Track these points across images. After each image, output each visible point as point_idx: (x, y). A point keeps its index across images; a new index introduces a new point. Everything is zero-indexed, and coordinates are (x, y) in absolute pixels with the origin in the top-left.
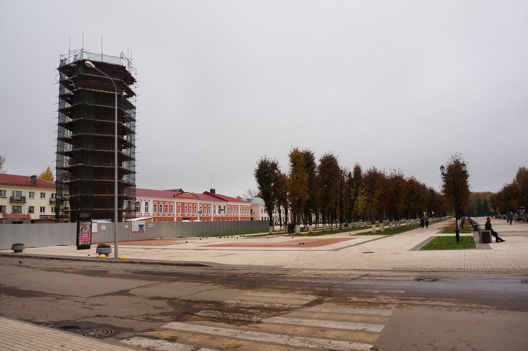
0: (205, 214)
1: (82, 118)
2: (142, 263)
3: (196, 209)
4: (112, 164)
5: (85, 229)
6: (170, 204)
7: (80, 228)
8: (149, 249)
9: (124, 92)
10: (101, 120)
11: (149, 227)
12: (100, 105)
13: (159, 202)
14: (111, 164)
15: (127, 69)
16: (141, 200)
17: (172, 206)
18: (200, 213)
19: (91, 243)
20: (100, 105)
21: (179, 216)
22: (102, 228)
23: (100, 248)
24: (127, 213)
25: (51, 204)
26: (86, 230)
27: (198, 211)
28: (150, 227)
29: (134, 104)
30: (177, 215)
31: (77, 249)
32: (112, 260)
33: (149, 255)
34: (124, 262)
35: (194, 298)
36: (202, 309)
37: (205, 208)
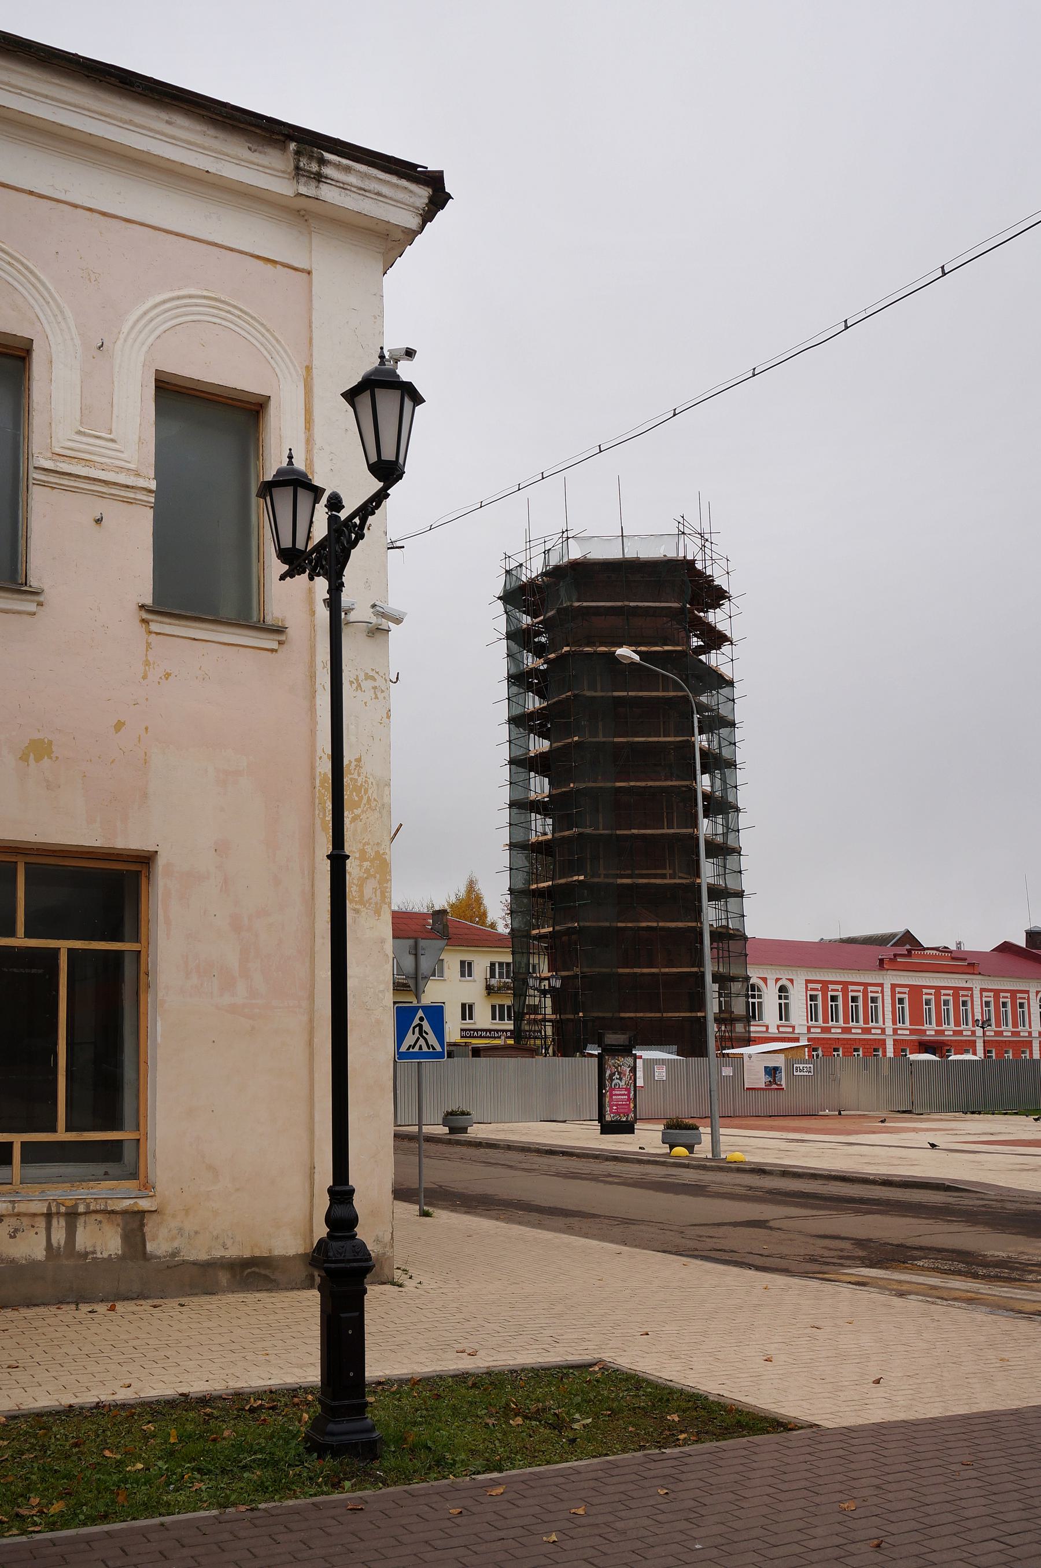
0: (1003, 1028)
1: (576, 739)
2: (786, 1173)
3: (970, 1010)
4: (671, 872)
5: (618, 1077)
6: (865, 993)
7: (608, 1073)
8: (803, 1141)
9: (695, 639)
10: (630, 739)
11: (798, 1073)
12: (625, 694)
13: (825, 984)
14: (668, 872)
15: (699, 566)
16: (765, 980)
17: (874, 1000)
18: (985, 1024)
19: (635, 1116)
20: (625, 694)
21: (904, 1034)
22: (656, 1074)
23: (672, 1131)
24: (723, 1028)
25: (489, 994)
26: (620, 1079)
27: (978, 1016)
28: (802, 1073)
29: (726, 670)
30: (895, 1031)
31: (601, 1133)
32: (708, 1164)
33: (804, 1157)
34: (739, 1170)
35: (909, 1242)
36: (926, 1258)
37: (1004, 1005)
